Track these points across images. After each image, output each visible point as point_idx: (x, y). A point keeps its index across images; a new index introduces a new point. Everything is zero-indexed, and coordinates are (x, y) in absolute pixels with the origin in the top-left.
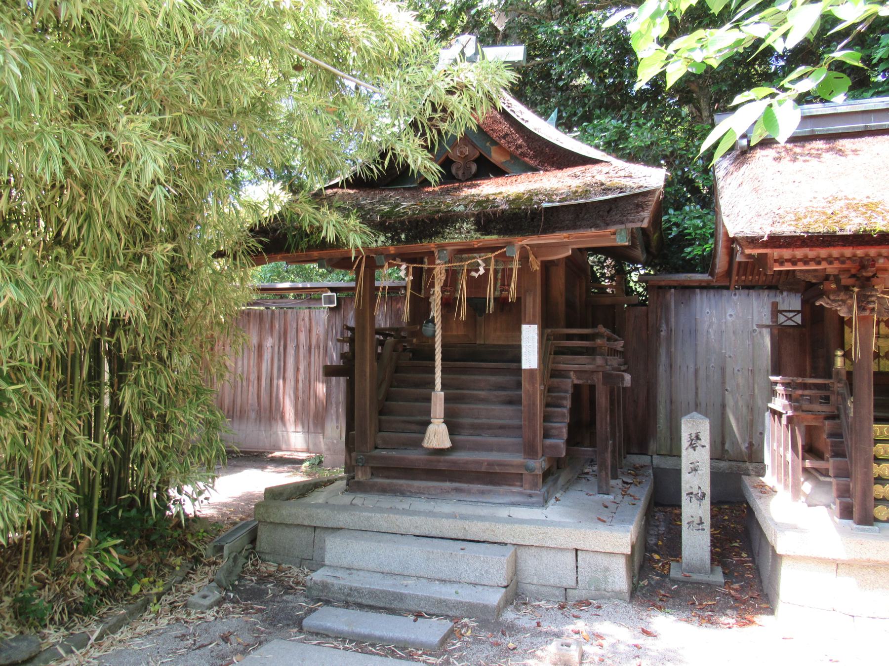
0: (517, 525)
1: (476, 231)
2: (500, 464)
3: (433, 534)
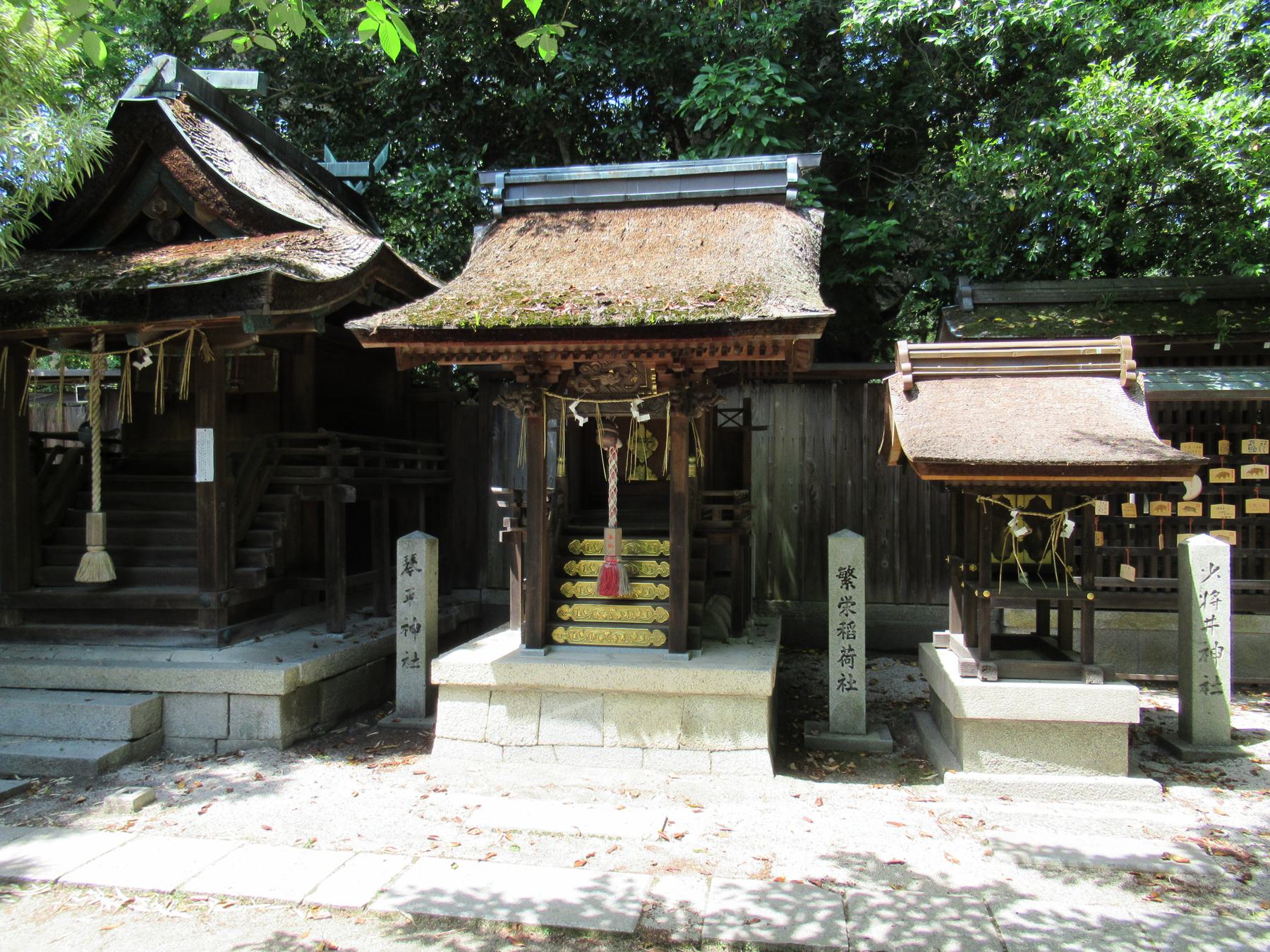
0: (162, 669)
1: (81, 314)
2: (172, 599)
3: (68, 686)
